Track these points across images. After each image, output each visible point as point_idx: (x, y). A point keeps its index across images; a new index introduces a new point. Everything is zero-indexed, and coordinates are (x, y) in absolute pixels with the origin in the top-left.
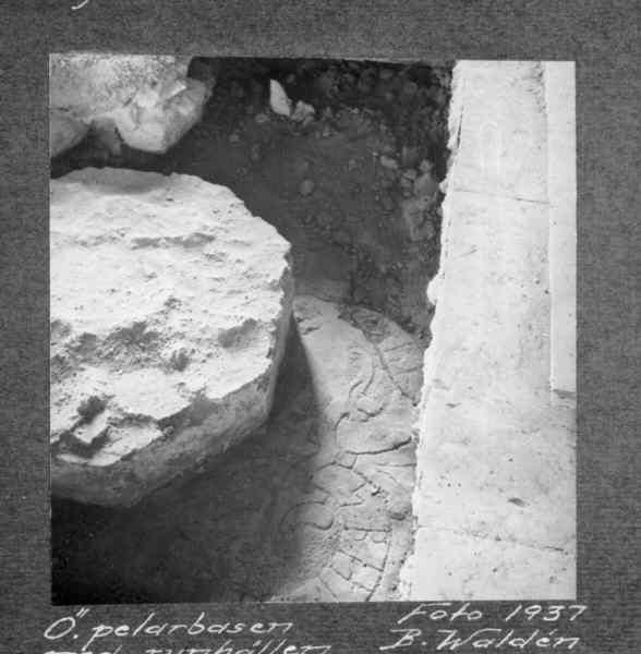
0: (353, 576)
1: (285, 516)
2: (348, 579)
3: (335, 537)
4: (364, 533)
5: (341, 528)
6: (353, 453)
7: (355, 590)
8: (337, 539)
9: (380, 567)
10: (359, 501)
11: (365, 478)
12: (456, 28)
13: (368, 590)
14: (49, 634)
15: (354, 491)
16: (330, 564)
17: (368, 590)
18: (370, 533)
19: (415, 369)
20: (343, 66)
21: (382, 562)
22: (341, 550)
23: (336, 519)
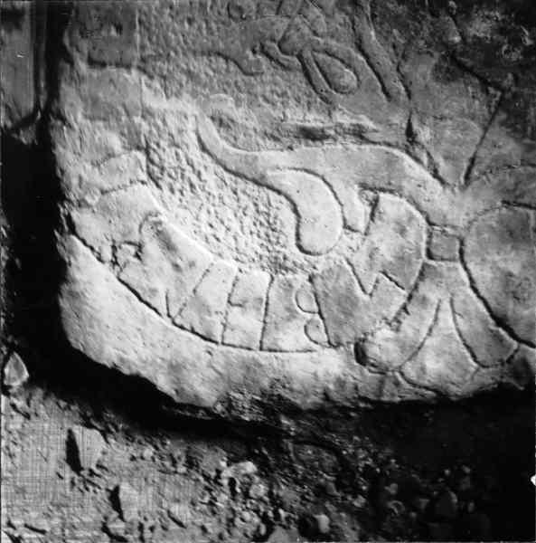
0: (236, 309)
1: (483, 138)
2: (229, 302)
3: (289, 264)
4: (315, 307)
5: (310, 270)
6: (461, 252)
7: (214, 316)
8: (286, 269)
9: (265, 347)
10: (369, 288)
11: (416, 287)
12: (310, 99)
13: (223, 337)
14: (94, 199)
15: (385, 273)
16: (245, 268)
17: (223, 337)
18: (317, 317)
19: (461, 252)
20: (257, 49)
21: (274, 347)
22: (273, 279)
23: (322, 258)
